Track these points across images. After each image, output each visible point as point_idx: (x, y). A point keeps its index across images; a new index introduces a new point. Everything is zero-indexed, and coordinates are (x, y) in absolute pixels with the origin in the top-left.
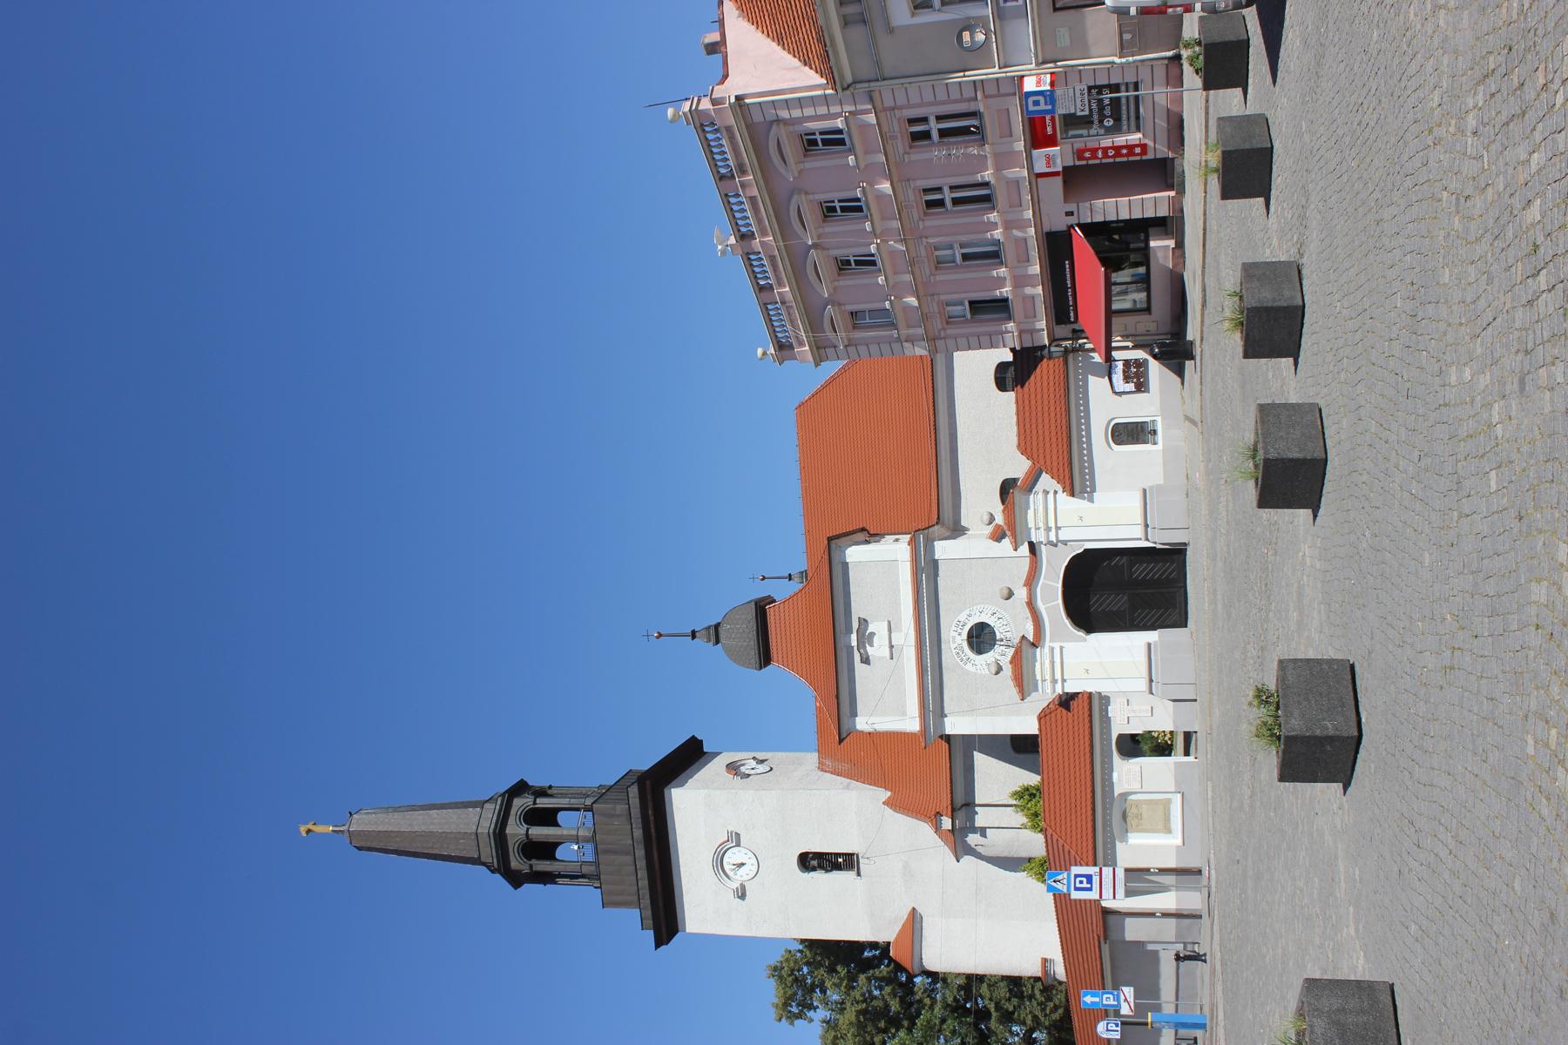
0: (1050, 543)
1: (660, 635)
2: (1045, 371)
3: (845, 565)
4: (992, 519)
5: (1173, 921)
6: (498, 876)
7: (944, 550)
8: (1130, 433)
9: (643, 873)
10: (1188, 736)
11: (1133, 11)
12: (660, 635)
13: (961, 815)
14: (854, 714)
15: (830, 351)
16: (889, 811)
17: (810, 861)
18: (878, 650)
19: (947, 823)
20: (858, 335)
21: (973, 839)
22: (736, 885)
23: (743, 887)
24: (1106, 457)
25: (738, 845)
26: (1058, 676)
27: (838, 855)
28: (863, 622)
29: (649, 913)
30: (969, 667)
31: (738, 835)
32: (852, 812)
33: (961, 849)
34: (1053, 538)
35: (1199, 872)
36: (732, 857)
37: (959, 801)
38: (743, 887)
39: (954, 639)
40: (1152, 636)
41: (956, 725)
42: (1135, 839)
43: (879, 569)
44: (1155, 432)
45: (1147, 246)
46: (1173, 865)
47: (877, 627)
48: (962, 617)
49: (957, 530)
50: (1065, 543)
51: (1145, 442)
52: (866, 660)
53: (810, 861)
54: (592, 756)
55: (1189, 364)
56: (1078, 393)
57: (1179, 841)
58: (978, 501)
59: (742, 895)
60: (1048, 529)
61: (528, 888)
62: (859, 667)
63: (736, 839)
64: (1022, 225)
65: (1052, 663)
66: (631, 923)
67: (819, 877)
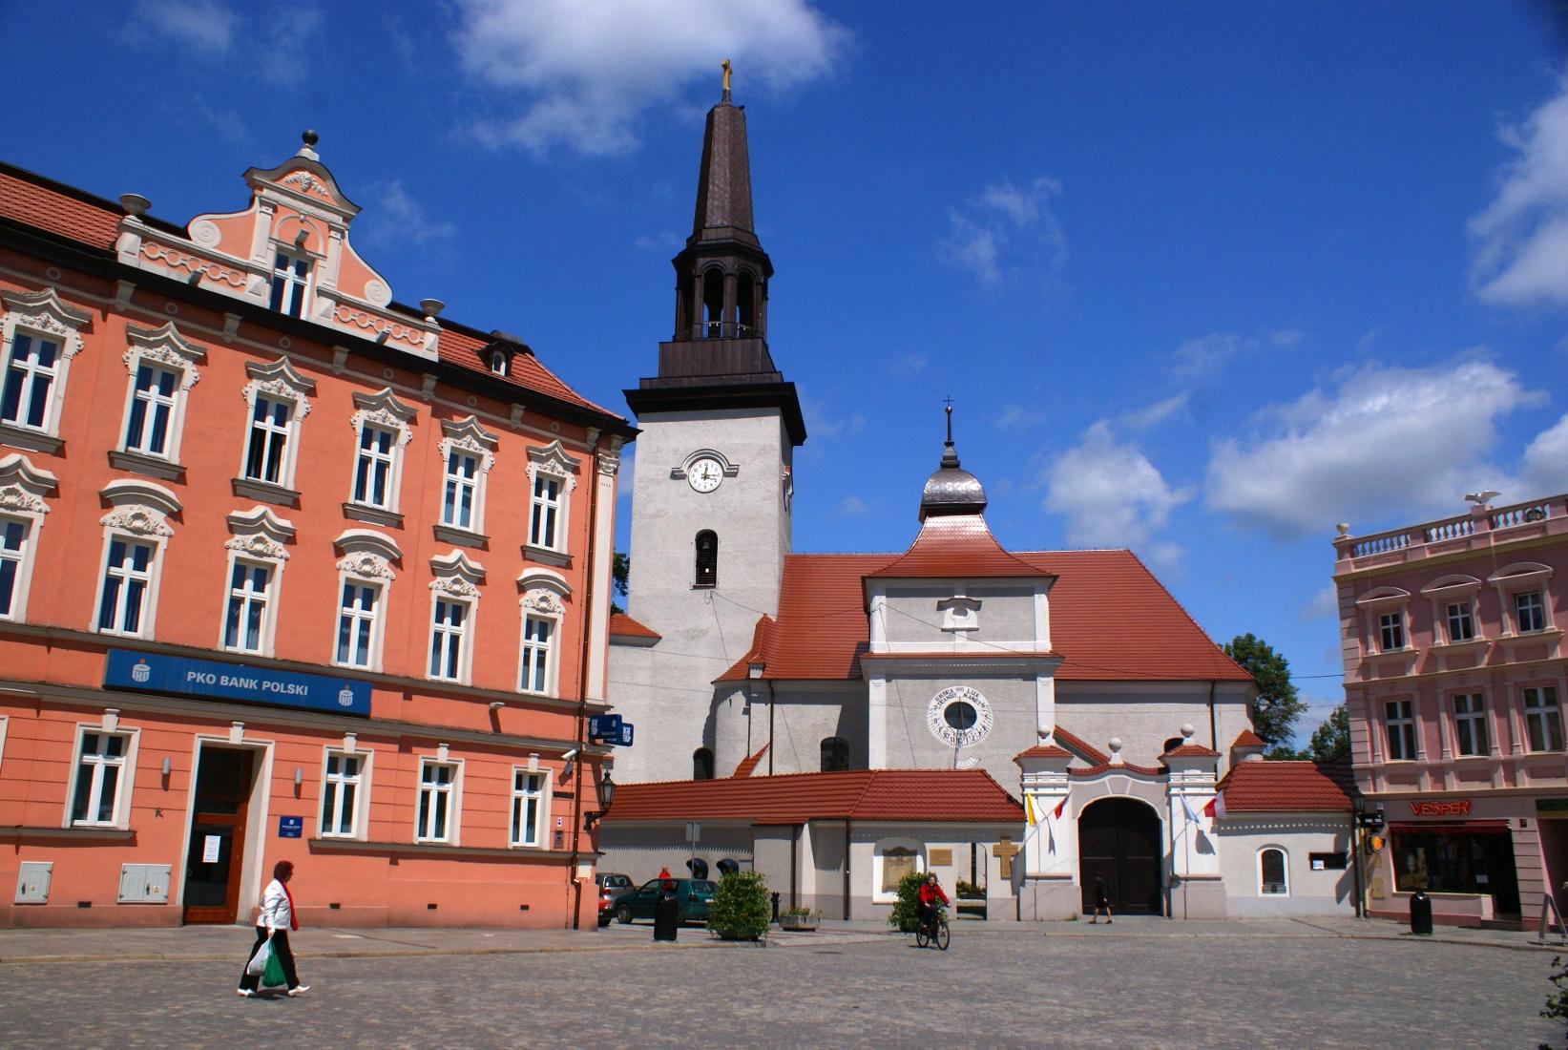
0: (1169, 789)
1: (949, 412)
2: (1327, 787)
3: (1030, 592)
4: (1188, 734)
5: (841, 892)
6: (683, 246)
7: (1046, 687)
8: (1273, 868)
9: (696, 382)
10: (981, 912)
11: (1020, 845)
12: (949, 412)
13: (764, 687)
14: (889, 594)
15: (1351, 592)
16: (758, 617)
17: (707, 545)
18: (950, 619)
19: (756, 674)
20: (1369, 617)
21: (739, 699)
22: (685, 469)
23: (684, 477)
24: (1250, 849)
25: (726, 475)
26: (1041, 791)
27: (714, 569)
28: (977, 607)
29: (655, 385)
30: (934, 702)
31: (735, 475)
32: (752, 580)
33: (723, 688)
34: (1174, 791)
35: (847, 916)
36: (714, 468)
37: (778, 687)
38: (684, 477)
39: (961, 691)
40: (1077, 880)
41: (878, 691)
42: (879, 862)
43: (1030, 625)
44: (1274, 890)
45: (1482, 889)
46: (854, 892)
47: (971, 619)
48: (982, 698)
49: (1060, 698)
50: (1169, 803)
51: (1265, 881)
52: (941, 607)
53: (707, 545)
54: (790, 343)
55: (1408, 928)
56: (1314, 820)
57: (876, 899)
58: (1090, 721)
59: (677, 475)
60: (1183, 787)
61: (672, 275)
62: (934, 601)
63: (731, 473)
64: (1511, 777)
65: (1055, 786)
66: (645, 367)
67: (690, 554)
